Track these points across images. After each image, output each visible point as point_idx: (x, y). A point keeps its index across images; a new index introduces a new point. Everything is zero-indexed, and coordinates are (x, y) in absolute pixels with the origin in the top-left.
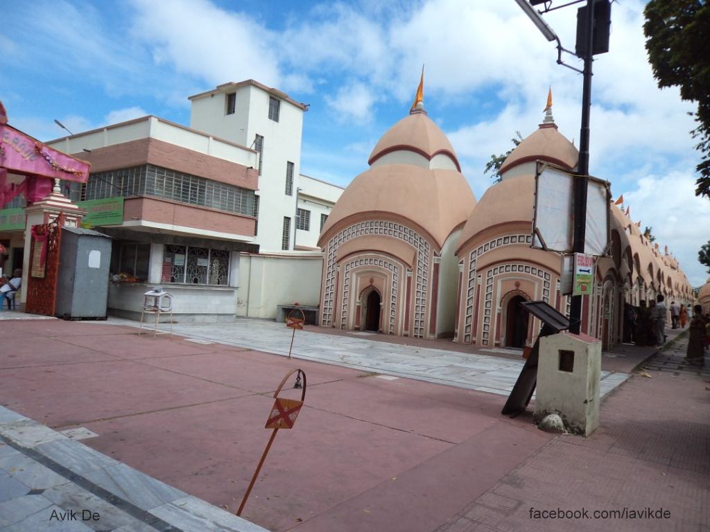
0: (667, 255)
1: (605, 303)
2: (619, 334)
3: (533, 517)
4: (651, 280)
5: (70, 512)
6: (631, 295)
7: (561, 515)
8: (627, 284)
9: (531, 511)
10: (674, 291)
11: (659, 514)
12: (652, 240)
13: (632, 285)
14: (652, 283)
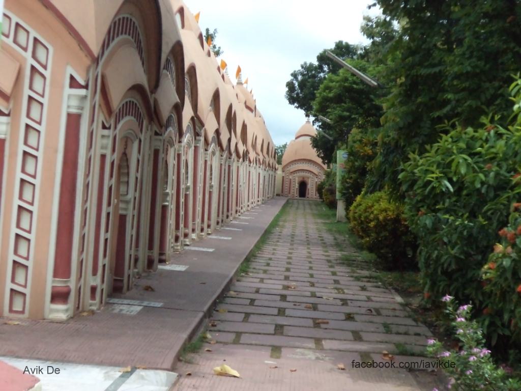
0: (240, 83)
1: (119, 174)
2: (258, 197)
4: (216, 126)
5: (438, 361)
6: (179, 155)
7: (381, 365)
8: (172, 131)
9: (353, 362)
10: (251, 150)
12: (217, 54)
13: (181, 134)
14: (217, 132)
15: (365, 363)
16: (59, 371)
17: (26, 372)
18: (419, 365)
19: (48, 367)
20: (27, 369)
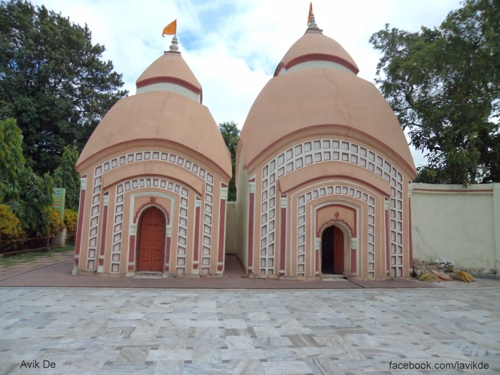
3: (392, 368)
5: (472, 363)
7: (412, 366)
11: (480, 366)
18: (454, 365)
20: (23, 364)
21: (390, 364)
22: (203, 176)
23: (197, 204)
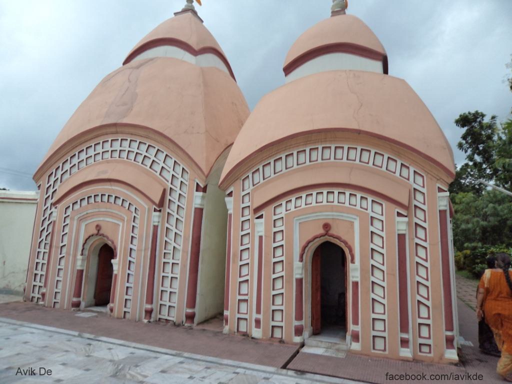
5: (30, 369)
7: (408, 377)
9: (387, 375)
11: (475, 377)
15: (398, 376)
16: (51, 372)
17: (18, 373)
19: (40, 368)
20: (19, 371)
21: (387, 375)
22: (407, 177)
23: (401, 224)
